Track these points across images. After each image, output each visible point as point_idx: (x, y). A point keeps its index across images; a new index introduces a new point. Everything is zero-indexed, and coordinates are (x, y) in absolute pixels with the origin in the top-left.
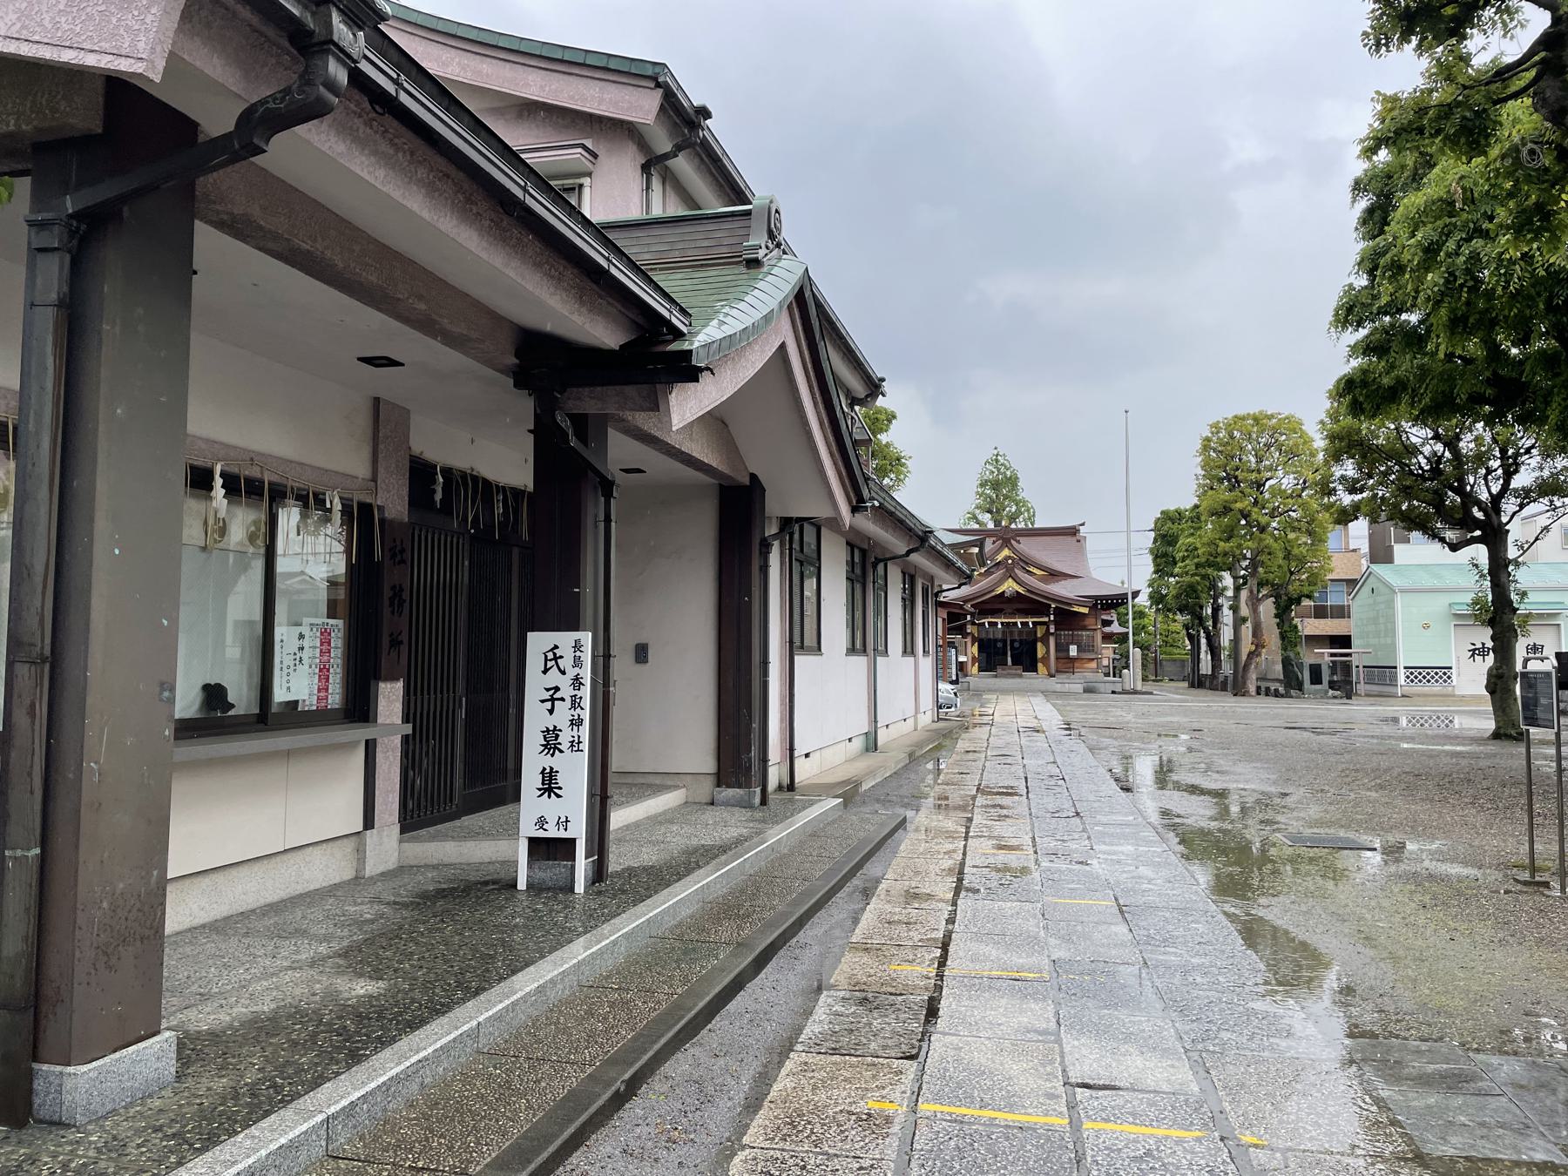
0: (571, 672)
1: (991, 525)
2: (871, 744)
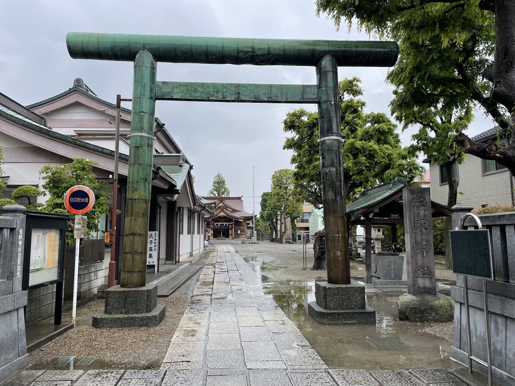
0: (154, 238)
1: (217, 195)
2: (191, 255)
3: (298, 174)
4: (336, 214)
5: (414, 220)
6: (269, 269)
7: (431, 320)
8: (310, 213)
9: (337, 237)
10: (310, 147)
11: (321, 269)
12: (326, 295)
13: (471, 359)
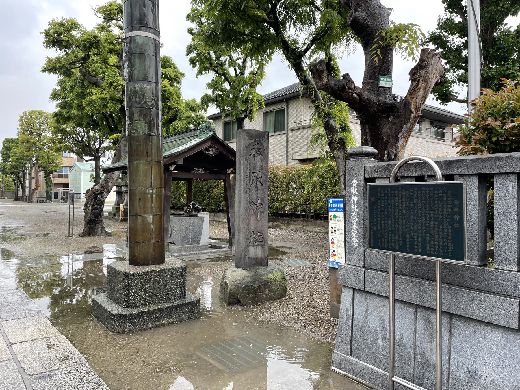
3: (60, 115)
4: (149, 159)
5: (250, 173)
6: (15, 239)
8: (71, 167)
9: (149, 193)
10: (84, 76)
11: (93, 235)
12: (128, 285)
13: (393, 382)
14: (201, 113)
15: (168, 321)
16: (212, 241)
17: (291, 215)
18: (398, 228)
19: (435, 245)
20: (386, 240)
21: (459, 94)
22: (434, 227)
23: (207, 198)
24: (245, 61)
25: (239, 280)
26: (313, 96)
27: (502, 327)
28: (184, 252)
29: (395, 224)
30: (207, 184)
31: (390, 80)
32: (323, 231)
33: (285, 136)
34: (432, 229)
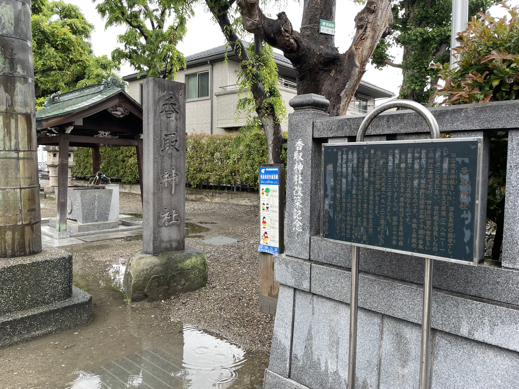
7: (180, 291)
14: (114, 71)
15: (44, 331)
16: (124, 216)
17: (216, 188)
18: (368, 209)
19: (425, 235)
20: (349, 227)
21: (394, 58)
22: (426, 209)
23: (123, 168)
24: (163, 13)
25: (147, 270)
26: (240, 55)
27: (508, 350)
28: (88, 230)
29: (363, 203)
30: (122, 153)
31: (333, 26)
32: (249, 204)
33: (210, 101)
34: (421, 211)
